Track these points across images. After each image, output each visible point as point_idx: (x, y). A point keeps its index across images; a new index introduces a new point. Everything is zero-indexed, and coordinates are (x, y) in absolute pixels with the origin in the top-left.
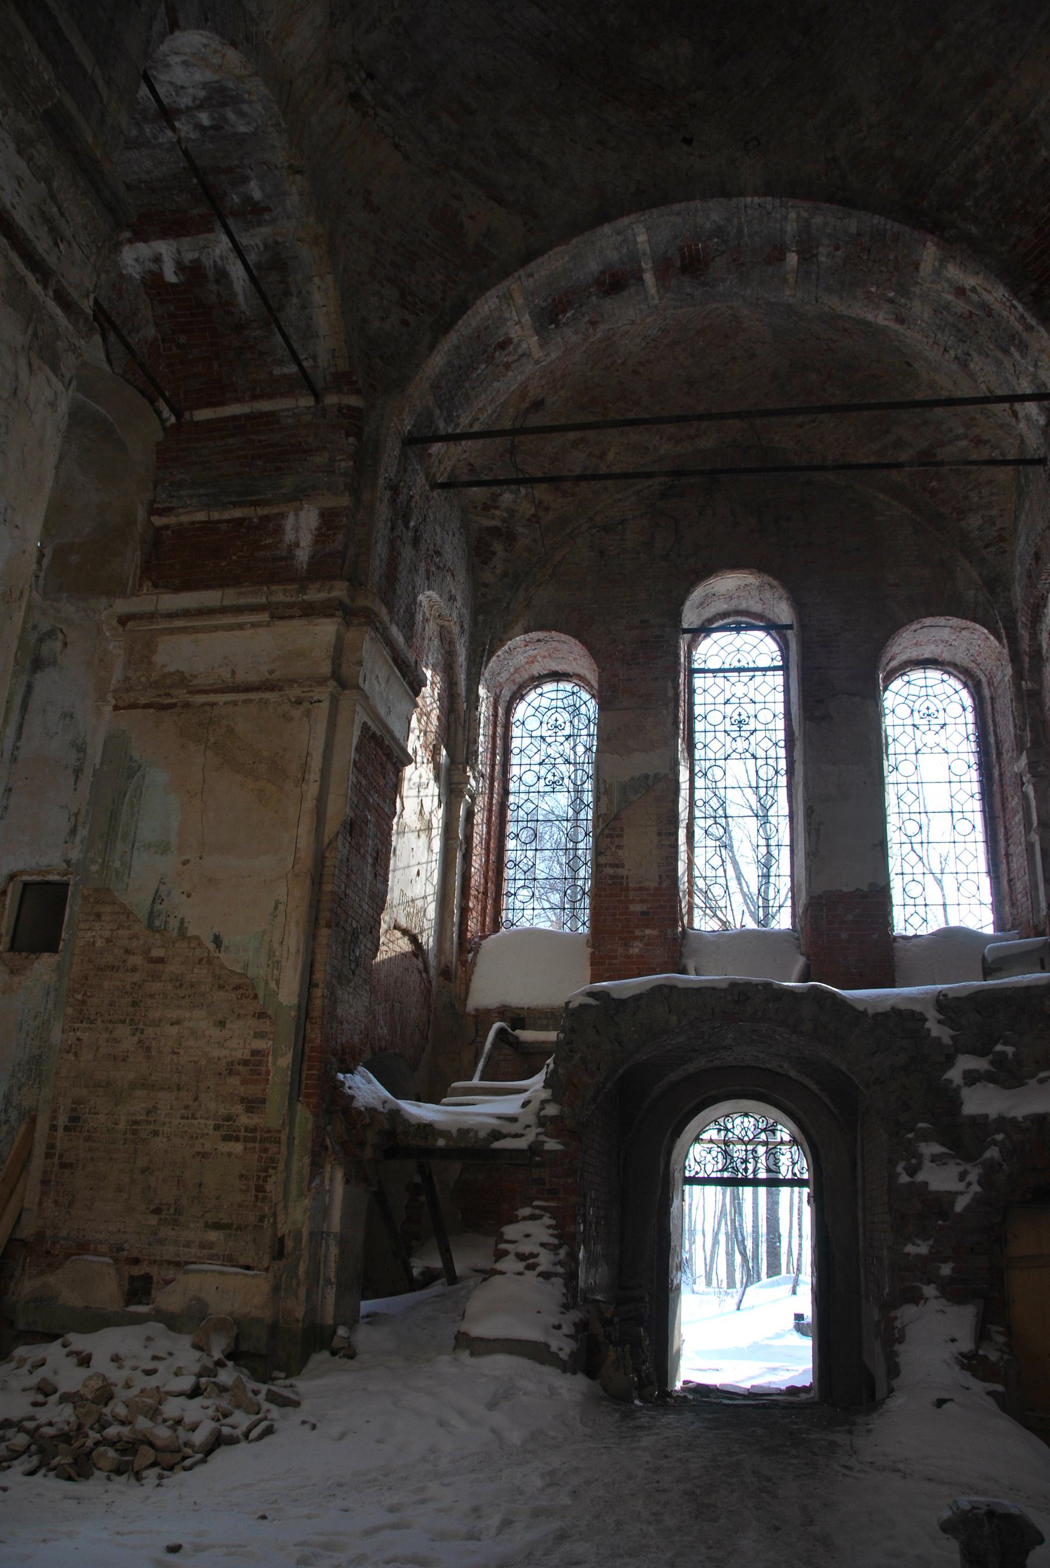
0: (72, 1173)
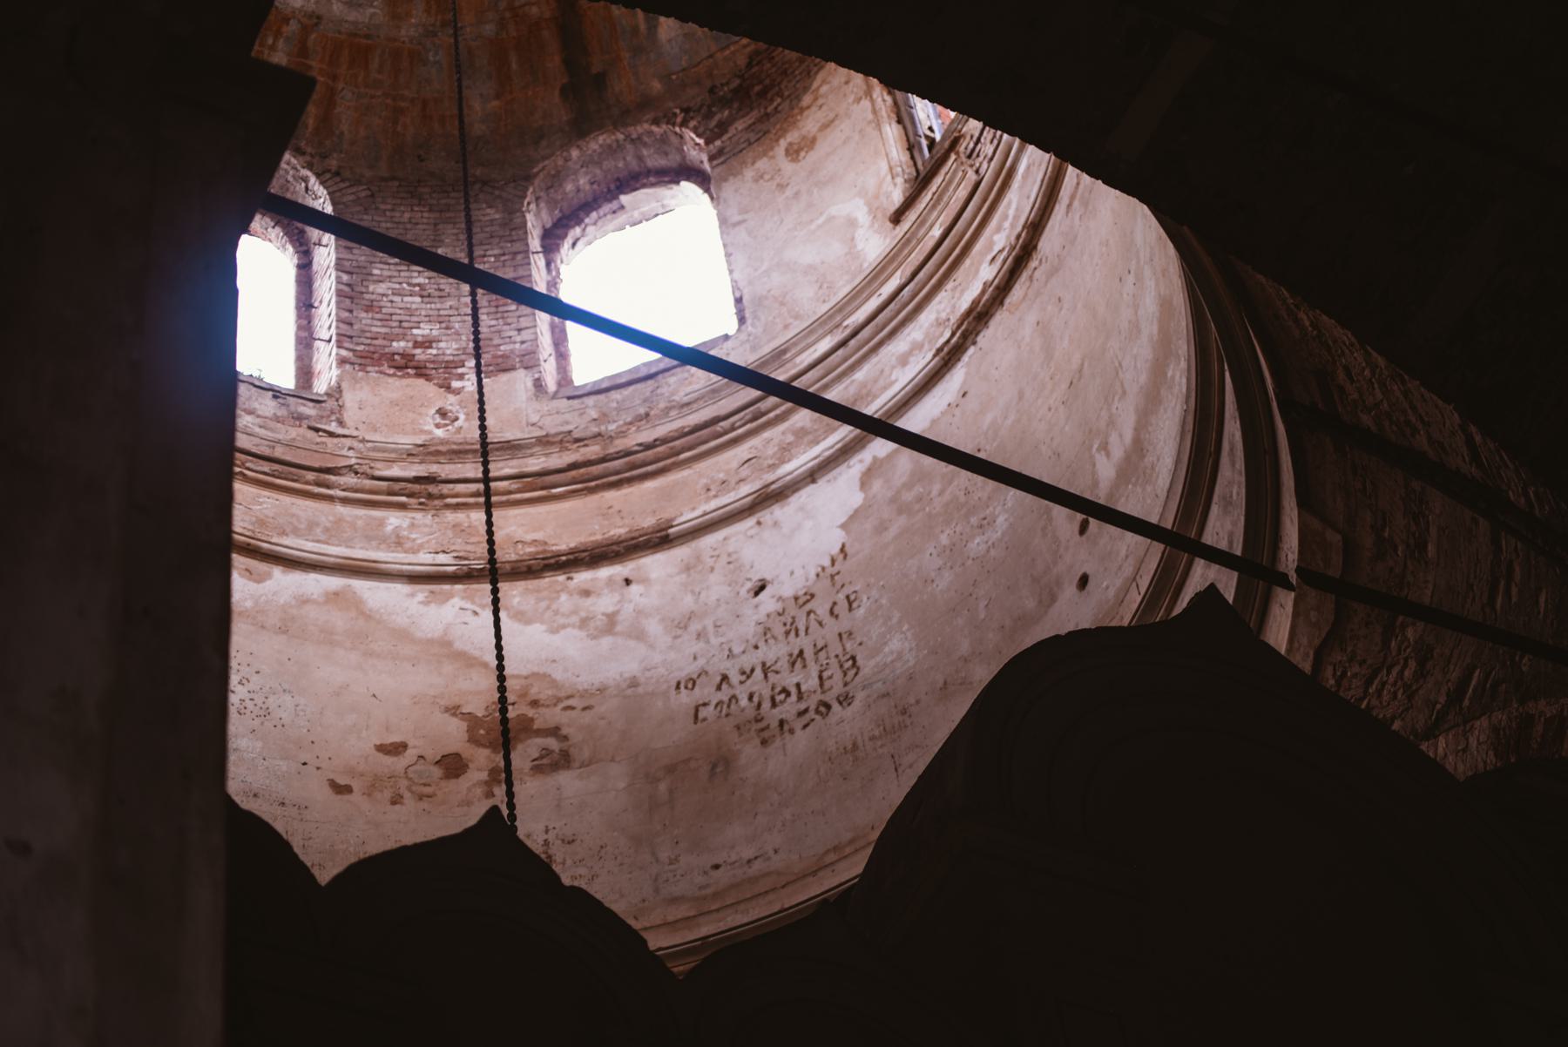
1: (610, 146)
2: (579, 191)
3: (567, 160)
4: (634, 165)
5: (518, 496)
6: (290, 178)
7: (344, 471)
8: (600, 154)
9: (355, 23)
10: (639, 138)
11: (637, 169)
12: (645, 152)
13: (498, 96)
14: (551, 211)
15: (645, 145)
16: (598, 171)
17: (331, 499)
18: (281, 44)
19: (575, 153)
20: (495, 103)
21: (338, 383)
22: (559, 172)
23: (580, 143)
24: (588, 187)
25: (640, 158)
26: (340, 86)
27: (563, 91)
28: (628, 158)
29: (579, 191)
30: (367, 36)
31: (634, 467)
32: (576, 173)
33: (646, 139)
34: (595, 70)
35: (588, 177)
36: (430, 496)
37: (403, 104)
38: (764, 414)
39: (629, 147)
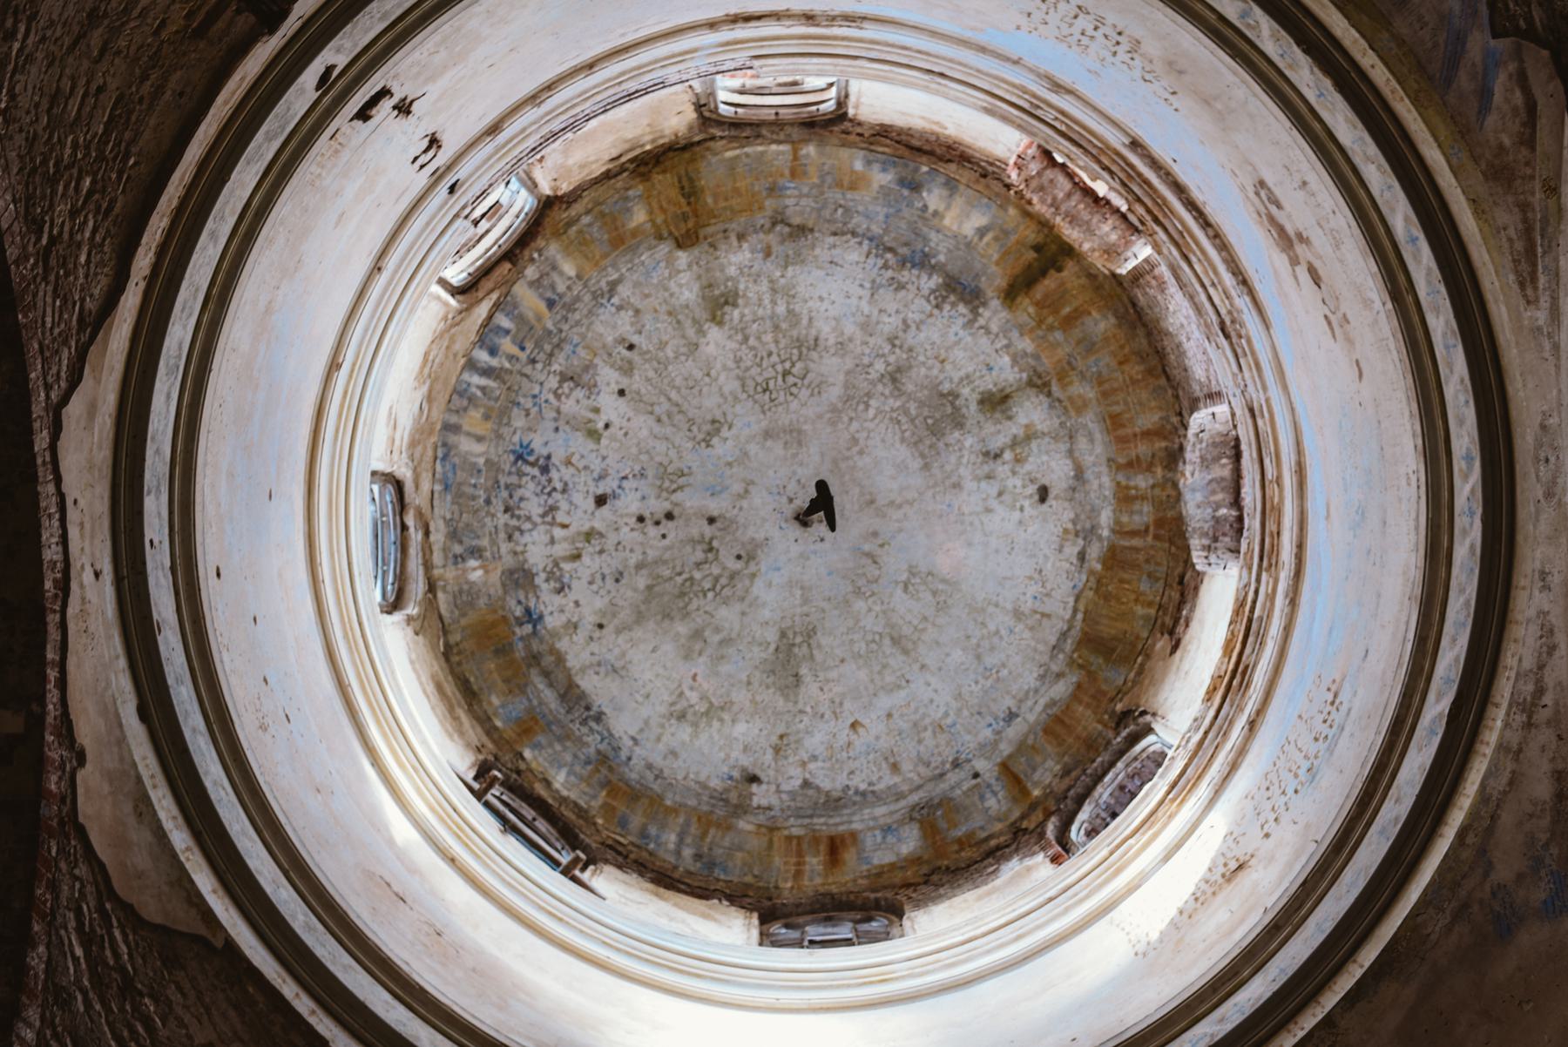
0: (1043, 494)
1: (1070, 222)
2: (1115, 228)
3: (1094, 250)
4: (1077, 196)
5: (1198, 253)
6: (1204, 445)
7: (1248, 397)
8: (1080, 226)
9: (1101, 432)
10: (1052, 205)
11: (1078, 193)
12: (1061, 195)
13: (1090, 313)
14: (1132, 243)
15: (1054, 199)
16: (1095, 220)
17: (1267, 400)
18: (1132, 483)
19: (1086, 246)
20: (1094, 313)
21: (606, 784)
22: (1105, 251)
23: (1076, 246)
24: (1110, 222)
25: (1069, 195)
26: (1137, 430)
27: (1059, 270)
28: (1073, 204)
29: (1115, 228)
30: (1105, 421)
31: (1129, 176)
32: (1101, 238)
33: (1049, 201)
34: (1035, 255)
35: (1102, 225)
36: (1233, 322)
37: (1127, 378)
38: (1031, 103)
39: (1063, 208)
